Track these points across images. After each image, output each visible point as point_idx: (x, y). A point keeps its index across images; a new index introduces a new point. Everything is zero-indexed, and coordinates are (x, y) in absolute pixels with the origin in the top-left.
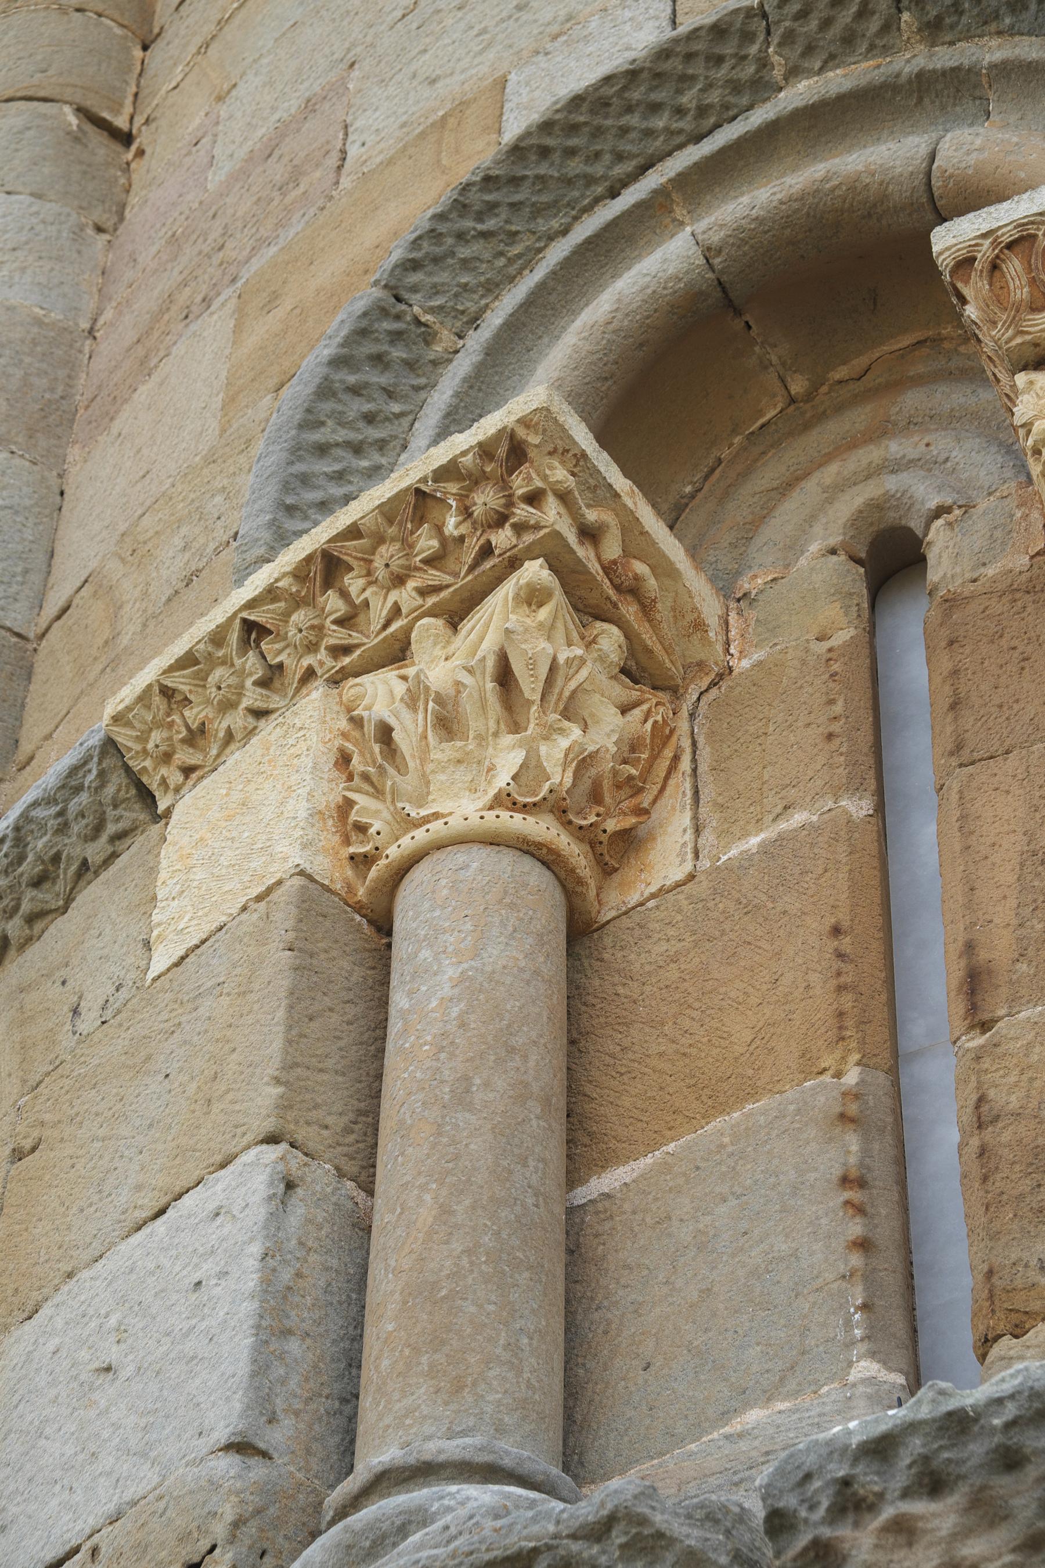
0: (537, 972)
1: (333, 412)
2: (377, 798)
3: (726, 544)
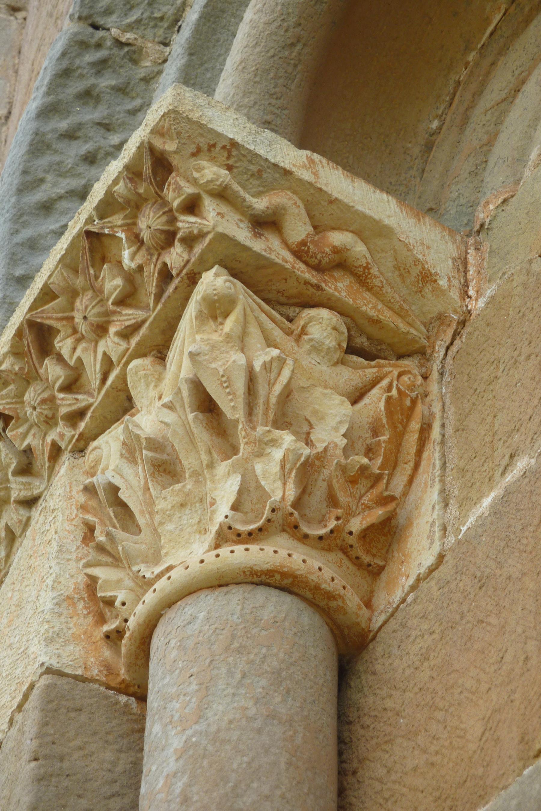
0: (271, 716)
1: (50, 165)
2: (117, 566)
3: (466, 175)
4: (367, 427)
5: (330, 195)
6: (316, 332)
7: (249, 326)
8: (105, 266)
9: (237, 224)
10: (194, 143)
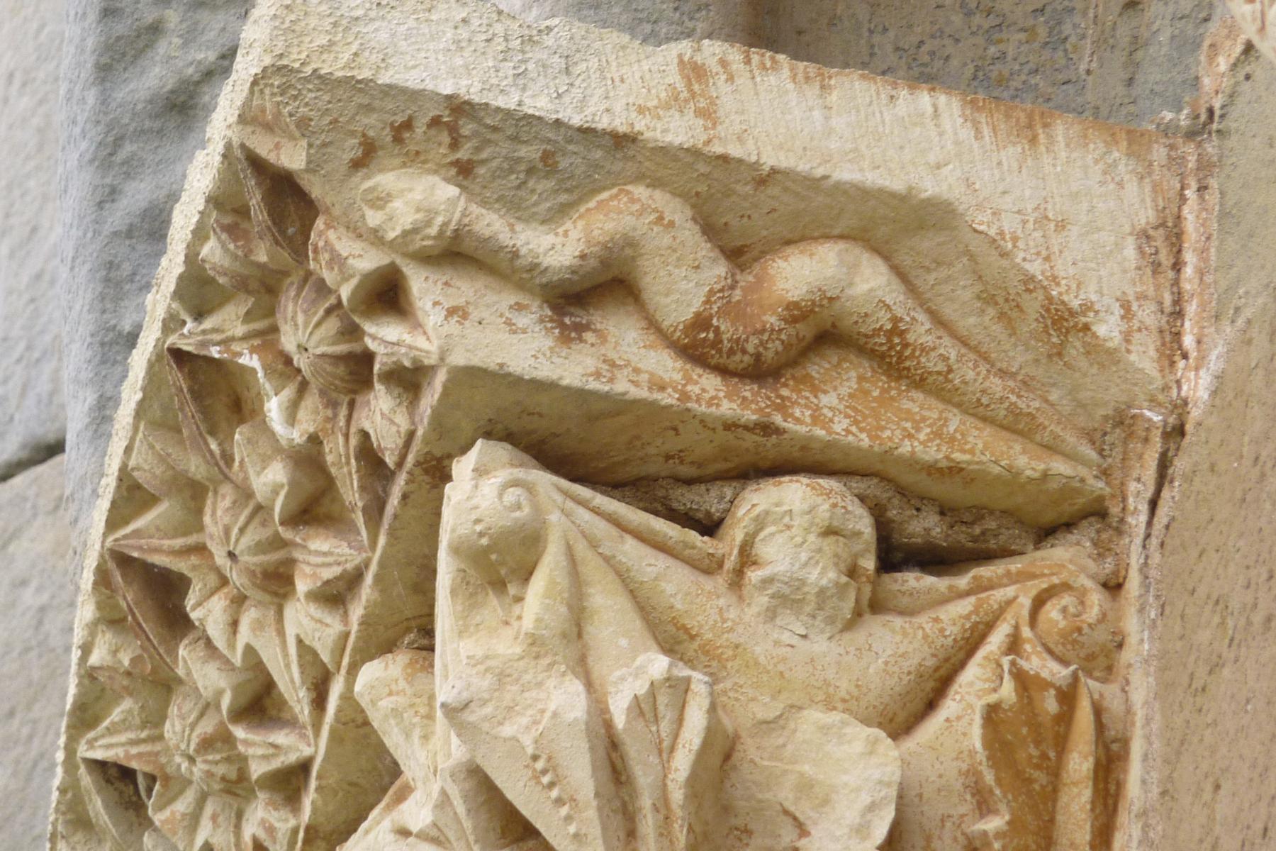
4: (958, 786)
5: (755, 166)
6: (780, 555)
7: (591, 591)
8: (237, 436)
9: (509, 323)
10: (352, 134)
